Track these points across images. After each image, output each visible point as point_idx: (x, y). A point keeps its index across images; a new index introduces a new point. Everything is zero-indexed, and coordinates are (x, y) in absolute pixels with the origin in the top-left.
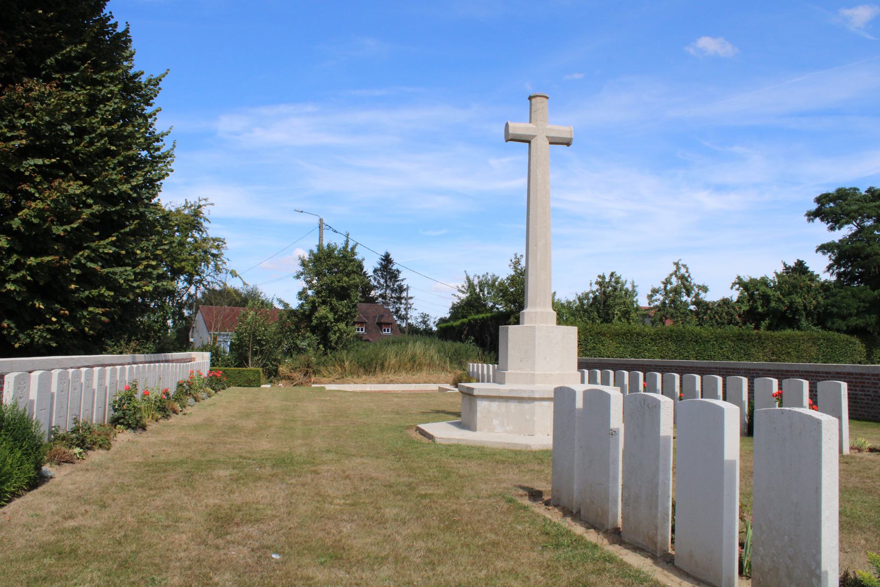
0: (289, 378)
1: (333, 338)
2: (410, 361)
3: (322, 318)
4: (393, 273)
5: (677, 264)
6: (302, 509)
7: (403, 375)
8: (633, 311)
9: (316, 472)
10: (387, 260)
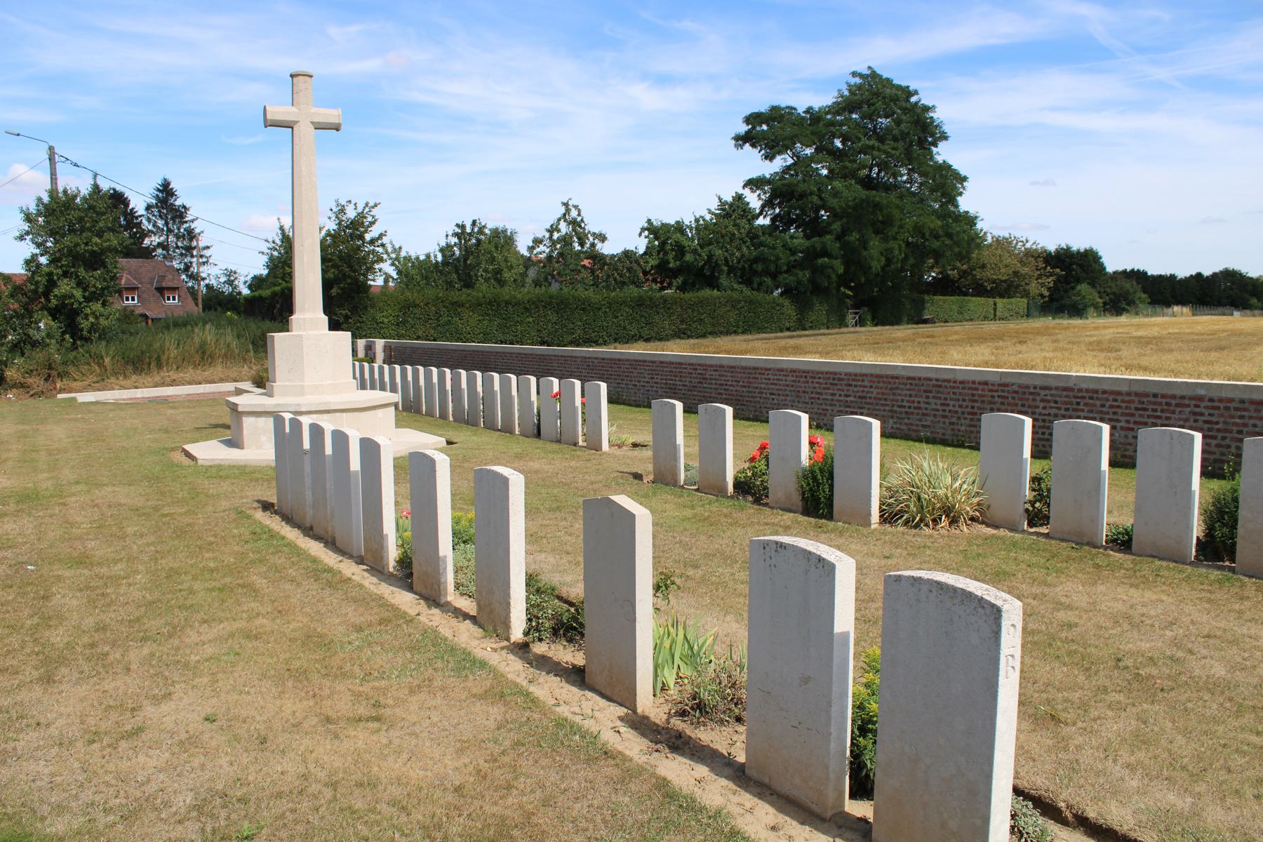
0: (22, 385)
1: (85, 324)
2: (197, 352)
3: (64, 297)
4: (177, 210)
5: (566, 205)
6: (51, 534)
7: (190, 373)
8: (505, 270)
9: (64, 504)
10: (166, 191)
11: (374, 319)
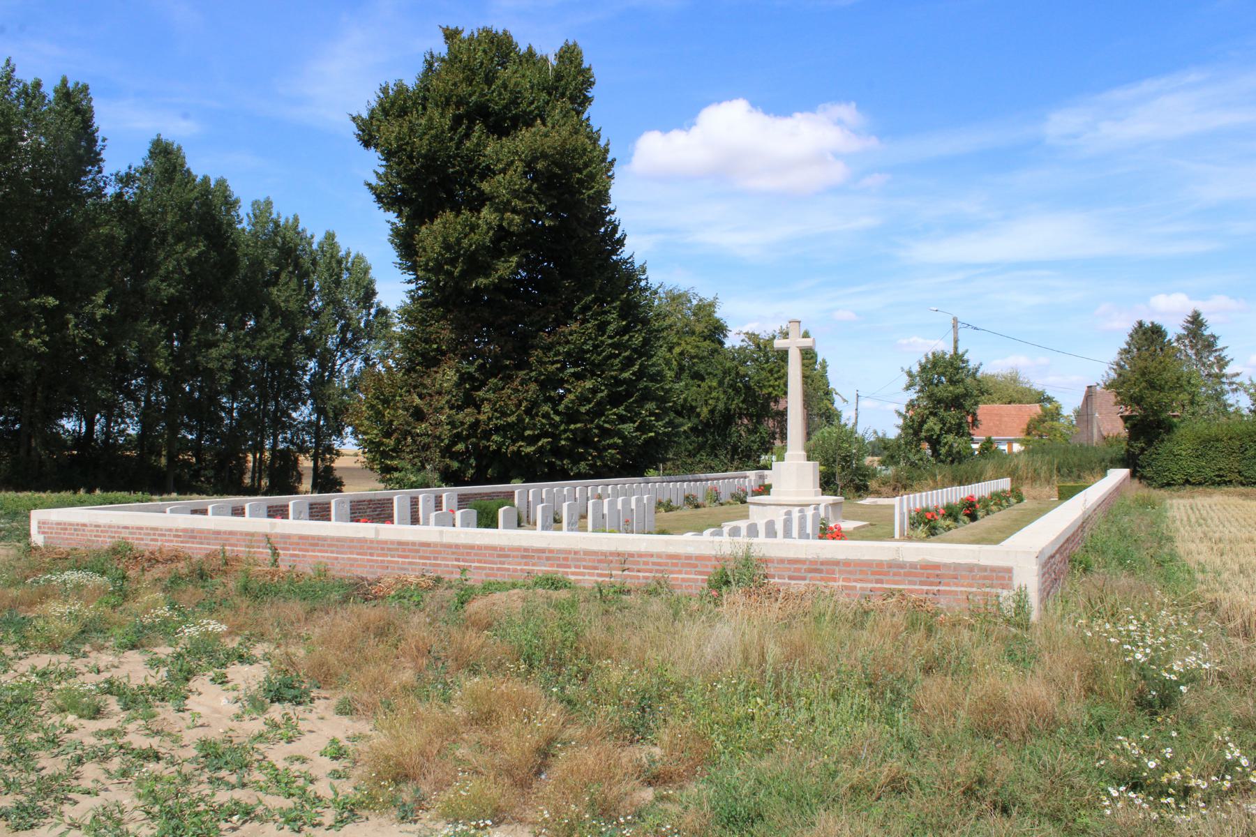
10: (1196, 322)
11: (1171, 451)
